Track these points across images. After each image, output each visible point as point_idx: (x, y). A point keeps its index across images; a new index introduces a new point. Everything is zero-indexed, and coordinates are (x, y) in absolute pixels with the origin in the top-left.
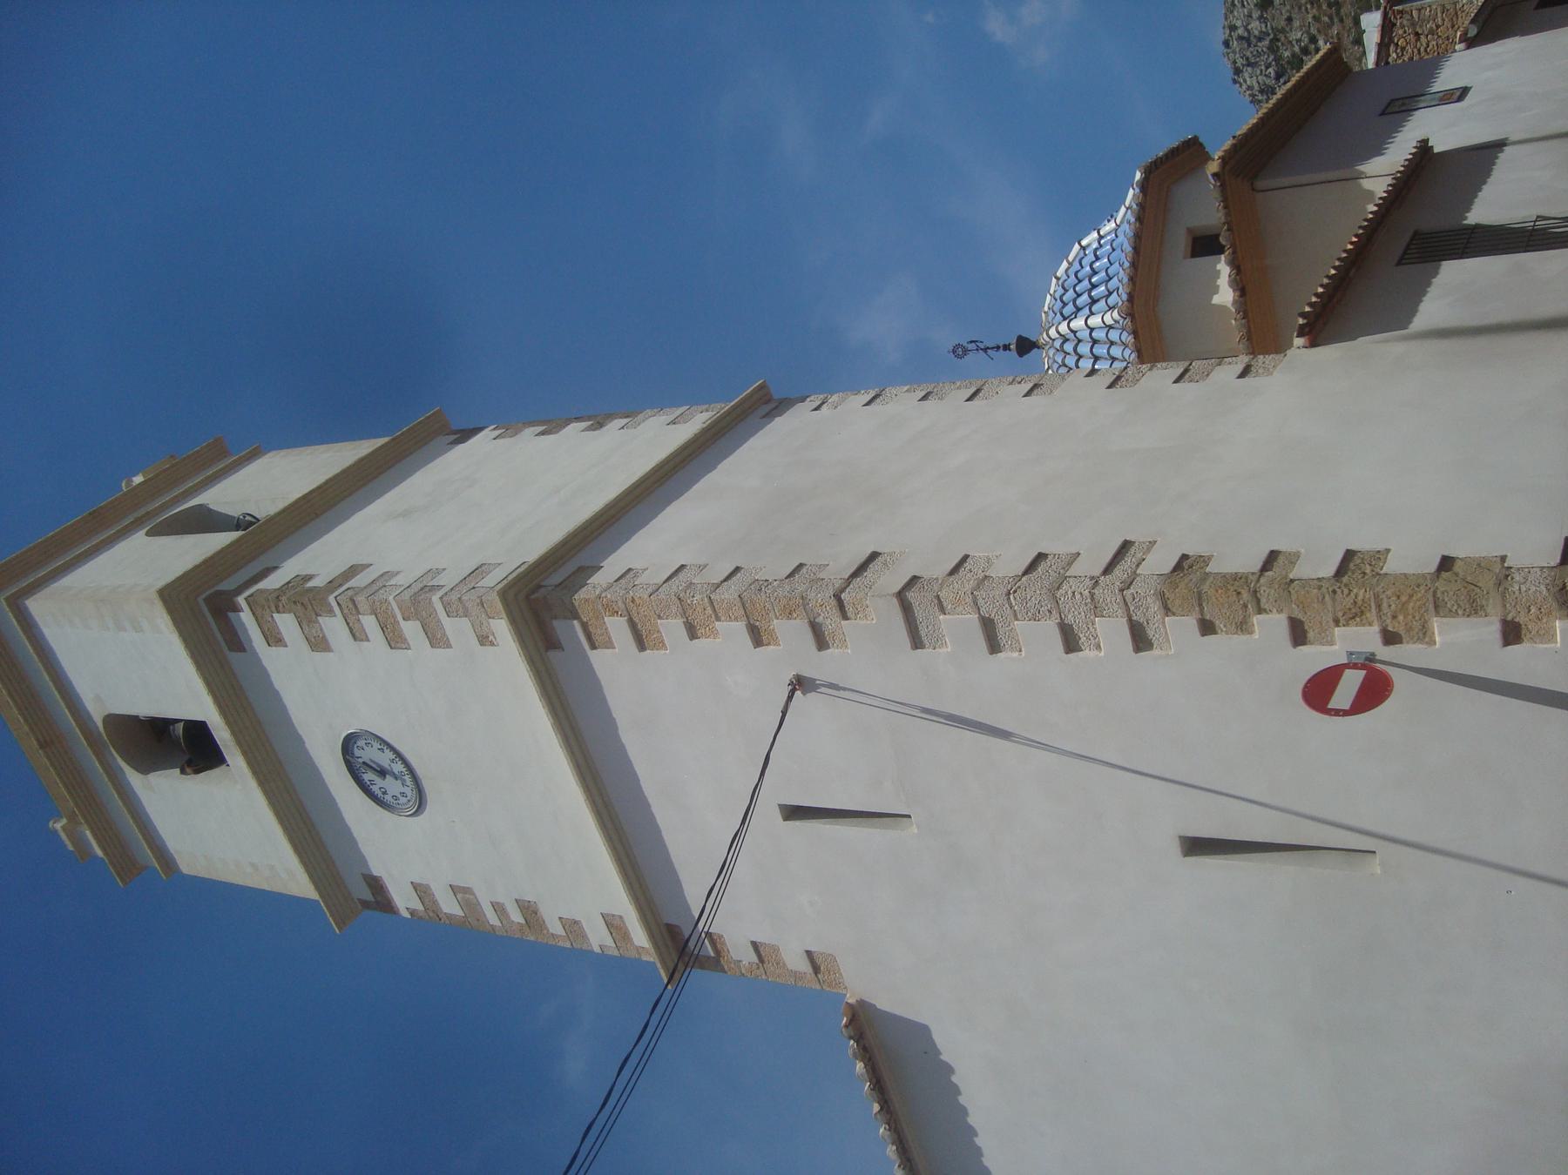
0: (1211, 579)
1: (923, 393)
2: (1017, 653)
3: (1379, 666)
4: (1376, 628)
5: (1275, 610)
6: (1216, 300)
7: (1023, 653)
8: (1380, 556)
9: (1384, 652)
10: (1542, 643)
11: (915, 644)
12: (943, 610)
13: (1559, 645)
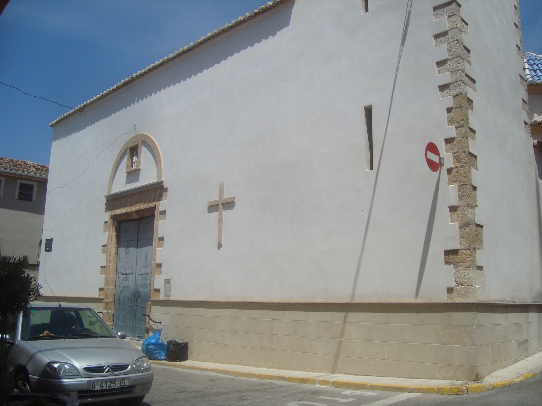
0: (466, 111)
1: (516, 6)
2: (435, 45)
3: (440, 167)
4: (453, 166)
5: (457, 133)
6: (536, 115)
7: (435, 47)
8: (476, 167)
9: (444, 169)
10: (450, 218)
11: (435, 8)
12: (449, 17)
13: (450, 223)
